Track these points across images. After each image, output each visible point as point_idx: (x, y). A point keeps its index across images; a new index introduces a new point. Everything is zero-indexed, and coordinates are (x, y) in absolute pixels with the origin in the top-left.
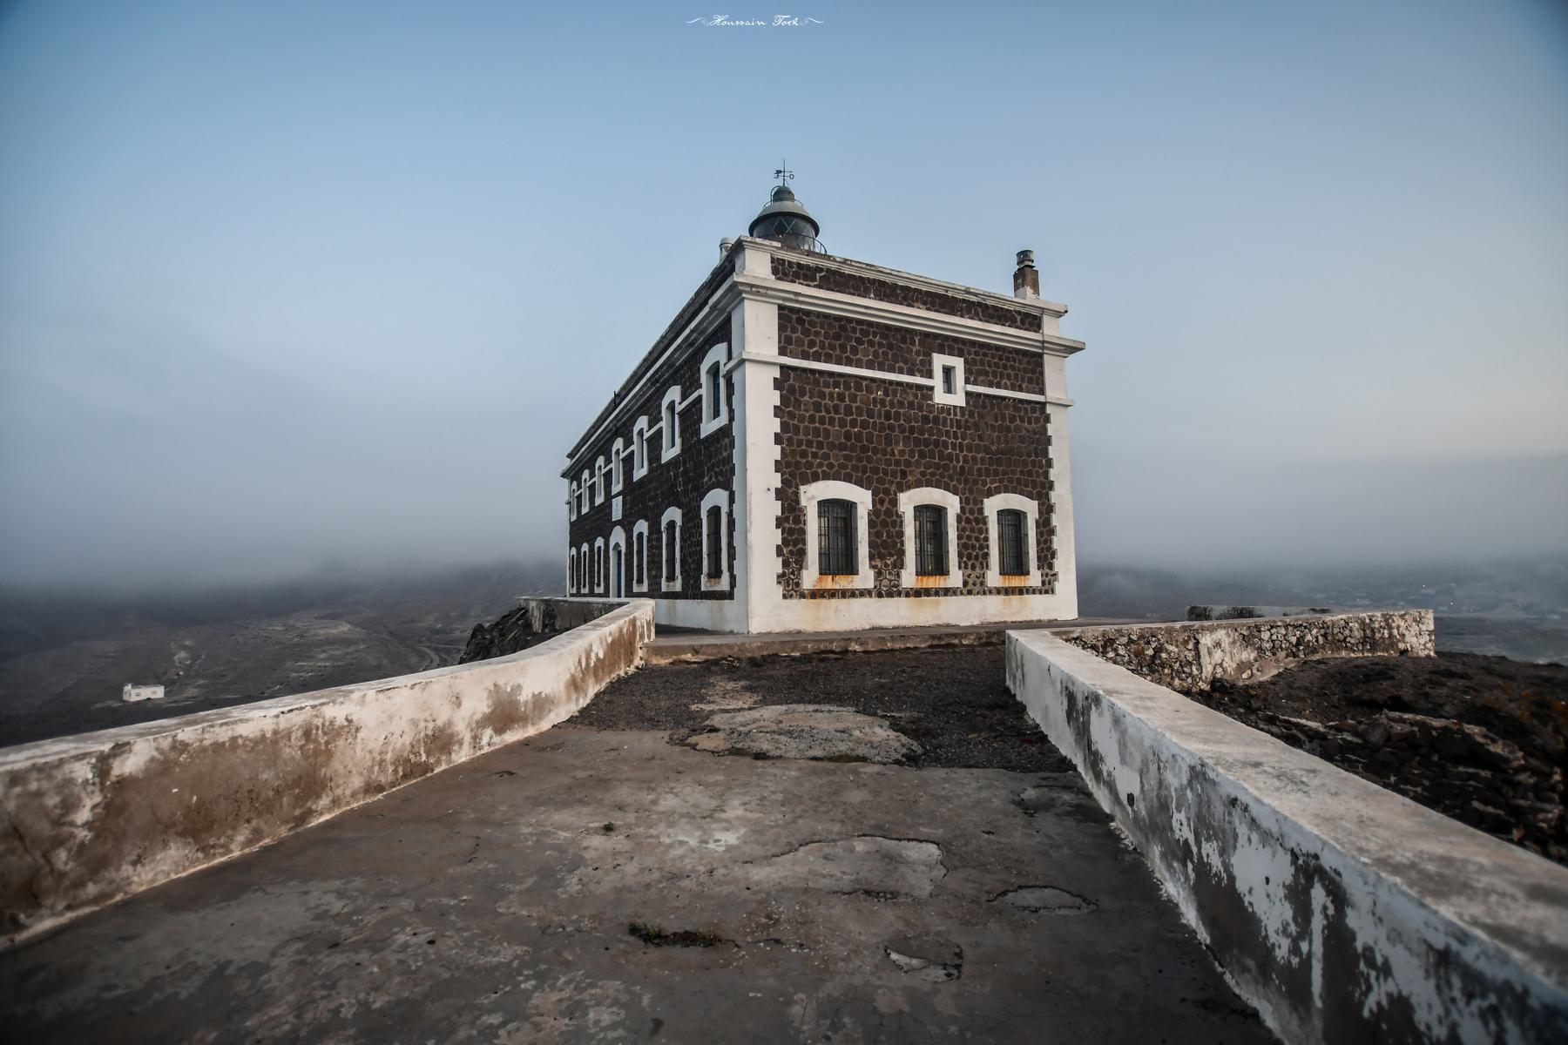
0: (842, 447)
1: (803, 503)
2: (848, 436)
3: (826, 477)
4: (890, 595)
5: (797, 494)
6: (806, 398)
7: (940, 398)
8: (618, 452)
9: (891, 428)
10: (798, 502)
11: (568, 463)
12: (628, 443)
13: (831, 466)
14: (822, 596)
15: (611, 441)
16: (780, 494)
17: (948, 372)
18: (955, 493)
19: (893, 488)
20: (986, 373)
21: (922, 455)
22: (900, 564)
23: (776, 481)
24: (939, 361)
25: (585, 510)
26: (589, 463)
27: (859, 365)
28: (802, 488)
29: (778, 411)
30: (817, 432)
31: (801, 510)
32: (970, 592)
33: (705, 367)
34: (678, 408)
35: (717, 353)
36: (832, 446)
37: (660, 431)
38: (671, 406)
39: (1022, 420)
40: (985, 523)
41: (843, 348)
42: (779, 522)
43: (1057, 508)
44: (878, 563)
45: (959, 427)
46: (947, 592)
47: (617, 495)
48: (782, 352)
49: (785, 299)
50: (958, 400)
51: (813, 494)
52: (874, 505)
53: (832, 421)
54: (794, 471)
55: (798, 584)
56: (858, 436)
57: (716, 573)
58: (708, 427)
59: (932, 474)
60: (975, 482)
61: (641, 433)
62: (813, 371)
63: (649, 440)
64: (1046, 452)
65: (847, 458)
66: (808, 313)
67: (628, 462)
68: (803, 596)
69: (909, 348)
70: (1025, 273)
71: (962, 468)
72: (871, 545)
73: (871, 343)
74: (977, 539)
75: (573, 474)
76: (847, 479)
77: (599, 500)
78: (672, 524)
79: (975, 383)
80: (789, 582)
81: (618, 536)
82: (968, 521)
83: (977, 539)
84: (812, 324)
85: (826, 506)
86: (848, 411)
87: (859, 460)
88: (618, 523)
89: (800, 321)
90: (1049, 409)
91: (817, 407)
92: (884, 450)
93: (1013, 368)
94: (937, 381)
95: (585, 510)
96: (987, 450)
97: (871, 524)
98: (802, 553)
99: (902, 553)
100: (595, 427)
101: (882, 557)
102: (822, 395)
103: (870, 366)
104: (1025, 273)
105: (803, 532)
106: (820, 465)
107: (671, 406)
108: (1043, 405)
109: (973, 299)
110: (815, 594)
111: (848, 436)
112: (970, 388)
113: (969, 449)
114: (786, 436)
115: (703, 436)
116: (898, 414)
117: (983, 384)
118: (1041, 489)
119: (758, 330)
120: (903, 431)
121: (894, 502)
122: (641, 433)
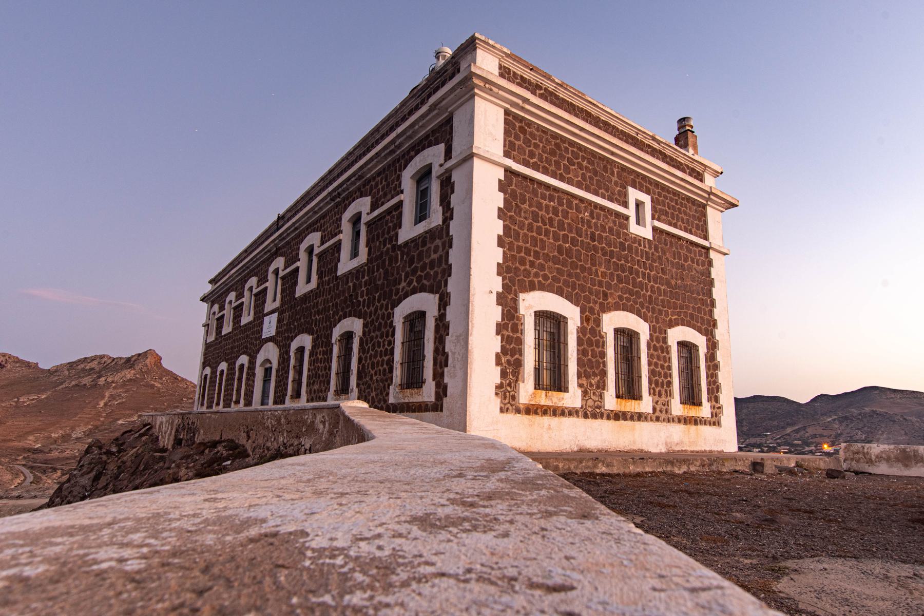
0: (556, 261)
1: (522, 311)
2: (560, 250)
3: (542, 288)
4: (594, 416)
5: (515, 300)
6: (526, 206)
7: (634, 228)
8: (230, 302)
9: (595, 249)
10: (516, 309)
11: (209, 288)
12: (240, 296)
13: (546, 277)
14: (536, 413)
15: (227, 292)
16: (501, 299)
17: (639, 205)
18: (646, 321)
19: (597, 307)
20: (666, 214)
21: (620, 280)
22: (602, 386)
23: (497, 284)
24: (634, 195)
25: (227, 329)
26: (238, 286)
27: (570, 182)
28: (522, 296)
29: (501, 214)
30: (534, 239)
31: (518, 319)
32: (658, 419)
33: (303, 246)
34: (281, 274)
35: (434, 155)
36: (547, 258)
37: (242, 303)
38: (276, 272)
39: (693, 261)
40: (668, 352)
41: (557, 164)
42: (500, 329)
43: (720, 345)
44: (584, 381)
45: (647, 259)
46: (640, 417)
47: (272, 312)
48: (507, 154)
49: (514, 104)
50: (646, 233)
51: (532, 302)
52: (582, 323)
53: (547, 233)
54: (514, 279)
55: (513, 398)
56: (569, 251)
57: (414, 381)
58: (408, 231)
59: (628, 300)
60: (660, 312)
61: (251, 289)
62: (532, 180)
63: (235, 308)
64: (710, 293)
65: (559, 271)
66: (530, 124)
67: (238, 310)
68: (518, 411)
69: (611, 177)
70: (684, 136)
71: (650, 297)
72: (580, 363)
73: (580, 166)
74: (662, 367)
75: (214, 298)
76: (560, 292)
77: (246, 319)
78: (301, 350)
79: (659, 220)
80: (506, 392)
81: (270, 352)
82: (655, 349)
83: (662, 367)
84: (533, 136)
85: (542, 316)
86: (561, 226)
87: (569, 275)
88: (270, 339)
89: (522, 130)
90: (712, 254)
91: (535, 217)
92: (590, 269)
93: (686, 214)
94: (631, 212)
95: (227, 329)
96: (669, 284)
97: (580, 342)
98: (518, 365)
99: (604, 373)
100: (247, 252)
101: (588, 376)
102: (539, 206)
103: (579, 185)
104: (684, 136)
105: (520, 342)
106: (536, 275)
107: (276, 272)
108: (707, 249)
109: (656, 145)
110: (531, 410)
111: (560, 250)
112: (658, 224)
113: (655, 281)
114: (507, 240)
115: (339, 273)
116: (600, 236)
117: (664, 222)
118: (708, 327)
119: (487, 125)
120: (604, 254)
121: (598, 322)
122: (251, 289)
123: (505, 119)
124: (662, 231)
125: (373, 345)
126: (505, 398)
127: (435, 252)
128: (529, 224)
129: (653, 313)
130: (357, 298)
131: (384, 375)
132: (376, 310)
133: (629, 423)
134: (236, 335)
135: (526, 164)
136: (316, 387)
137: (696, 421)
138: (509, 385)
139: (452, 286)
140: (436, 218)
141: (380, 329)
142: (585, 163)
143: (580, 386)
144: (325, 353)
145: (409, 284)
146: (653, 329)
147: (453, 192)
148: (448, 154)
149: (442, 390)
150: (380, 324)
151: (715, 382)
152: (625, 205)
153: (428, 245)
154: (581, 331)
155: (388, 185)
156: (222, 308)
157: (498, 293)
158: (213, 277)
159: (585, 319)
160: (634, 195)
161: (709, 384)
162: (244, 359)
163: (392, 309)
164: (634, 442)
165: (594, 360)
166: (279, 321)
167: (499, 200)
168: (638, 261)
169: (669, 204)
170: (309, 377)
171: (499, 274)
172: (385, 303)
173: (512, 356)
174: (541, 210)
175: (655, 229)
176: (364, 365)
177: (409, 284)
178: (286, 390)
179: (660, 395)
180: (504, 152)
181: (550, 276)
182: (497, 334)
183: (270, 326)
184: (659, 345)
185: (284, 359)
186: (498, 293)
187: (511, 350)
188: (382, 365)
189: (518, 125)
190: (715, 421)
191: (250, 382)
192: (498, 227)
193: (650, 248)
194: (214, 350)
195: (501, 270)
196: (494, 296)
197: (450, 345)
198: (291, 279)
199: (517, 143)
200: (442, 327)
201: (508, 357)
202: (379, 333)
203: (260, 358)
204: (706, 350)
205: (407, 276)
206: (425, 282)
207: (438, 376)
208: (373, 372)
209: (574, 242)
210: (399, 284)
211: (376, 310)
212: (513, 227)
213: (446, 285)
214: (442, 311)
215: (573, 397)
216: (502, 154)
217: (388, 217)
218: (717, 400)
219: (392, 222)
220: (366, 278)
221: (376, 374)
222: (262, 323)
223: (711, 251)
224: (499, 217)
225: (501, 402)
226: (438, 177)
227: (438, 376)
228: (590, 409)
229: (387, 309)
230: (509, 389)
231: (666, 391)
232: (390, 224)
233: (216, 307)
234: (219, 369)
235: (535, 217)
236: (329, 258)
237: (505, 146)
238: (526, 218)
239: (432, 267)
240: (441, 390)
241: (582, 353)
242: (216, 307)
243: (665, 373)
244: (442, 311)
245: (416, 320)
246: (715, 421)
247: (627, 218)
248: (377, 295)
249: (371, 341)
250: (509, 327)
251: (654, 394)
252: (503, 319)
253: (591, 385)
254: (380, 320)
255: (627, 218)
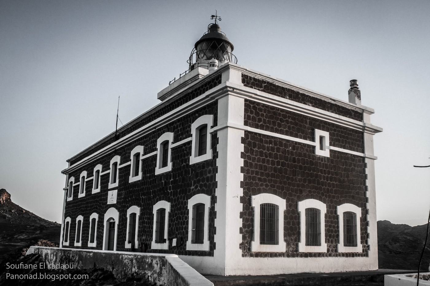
0: (273, 175)
4: (293, 256)
7: (319, 152)
15: (81, 170)
16: (242, 200)
18: (324, 203)
24: (318, 133)
28: (253, 197)
30: (261, 166)
32: (330, 255)
35: (207, 119)
42: (242, 215)
44: (288, 238)
46: (320, 255)
48: (246, 124)
51: (258, 200)
54: (250, 187)
57: (198, 239)
58: (194, 160)
69: (305, 126)
74: (334, 227)
81: (113, 214)
90: (367, 161)
92: (292, 178)
94: (317, 144)
98: (252, 233)
102: (264, 148)
108: (364, 158)
119: (234, 110)
123: (245, 104)
124: (335, 151)
125: (177, 218)
126: (244, 250)
127: (209, 173)
128: (258, 158)
129: (329, 198)
130: (167, 190)
131: (183, 235)
132: (178, 198)
133: (313, 258)
134: (88, 199)
135: (257, 127)
136: (144, 238)
137: (353, 255)
138: (247, 243)
139: (218, 193)
140: (208, 156)
141: (179, 212)
142: (290, 120)
143: (285, 240)
144: (149, 219)
145: (196, 187)
146: (328, 207)
147: (218, 143)
148: (215, 123)
149: (213, 246)
150: (181, 207)
151: (366, 232)
152: (313, 140)
153: (206, 169)
154: (286, 213)
155: (184, 129)
156: (77, 180)
157: (241, 197)
158: (70, 158)
159: (289, 205)
160: (318, 133)
161: (362, 234)
162: (95, 216)
163: (187, 200)
164: (311, 270)
165: (293, 226)
166: (119, 195)
167: (241, 148)
168: (321, 170)
169: (340, 135)
170: (139, 231)
171: (241, 187)
172: (183, 195)
173: (248, 228)
174: (264, 150)
175: (331, 151)
176: (172, 228)
177: (196, 187)
178: (125, 237)
179: (332, 242)
180: (245, 121)
181: (269, 184)
182: (241, 217)
183: (112, 197)
184: (332, 217)
185: (123, 218)
186: (241, 197)
187: (248, 225)
188: (182, 230)
189: (252, 105)
190: (365, 253)
191: (101, 230)
192: (241, 162)
193: (328, 162)
194: (73, 206)
195: (243, 185)
196: (239, 198)
197: (217, 223)
198: (125, 172)
199: (251, 115)
200: (213, 214)
201: (246, 229)
202: (180, 212)
203: (107, 217)
204: (361, 216)
205: (195, 183)
206: (204, 188)
207: (211, 238)
208: (177, 233)
209: (283, 164)
210: (191, 187)
211: (178, 198)
212: (249, 161)
213: (215, 192)
214: (213, 205)
215: (281, 246)
216: (243, 123)
217: (184, 147)
218: (367, 242)
219: (186, 150)
220: (172, 179)
221: (179, 234)
222: (107, 194)
223: (366, 159)
224: (242, 157)
225: (243, 251)
226: (211, 133)
227: (211, 238)
228: (291, 253)
229: (184, 199)
230: (246, 245)
231: (336, 240)
232: (185, 152)
233: (72, 179)
234: (78, 219)
235: (261, 153)
236: (149, 164)
237: (245, 118)
238: (256, 155)
239: (208, 181)
240: (213, 246)
241: (286, 223)
242: (72, 179)
243: (335, 230)
244: (213, 205)
245: (199, 208)
246: (365, 253)
247: (314, 147)
248: (179, 190)
249: (176, 215)
250: (247, 213)
251: (329, 242)
252: (243, 210)
253: (292, 240)
254: (181, 205)
255: (314, 147)
